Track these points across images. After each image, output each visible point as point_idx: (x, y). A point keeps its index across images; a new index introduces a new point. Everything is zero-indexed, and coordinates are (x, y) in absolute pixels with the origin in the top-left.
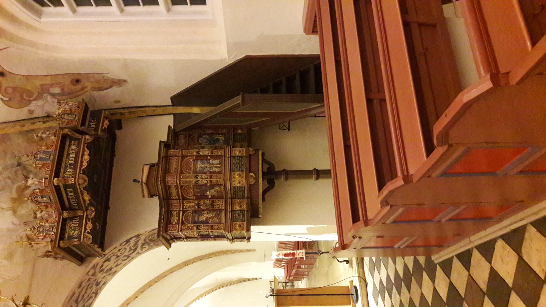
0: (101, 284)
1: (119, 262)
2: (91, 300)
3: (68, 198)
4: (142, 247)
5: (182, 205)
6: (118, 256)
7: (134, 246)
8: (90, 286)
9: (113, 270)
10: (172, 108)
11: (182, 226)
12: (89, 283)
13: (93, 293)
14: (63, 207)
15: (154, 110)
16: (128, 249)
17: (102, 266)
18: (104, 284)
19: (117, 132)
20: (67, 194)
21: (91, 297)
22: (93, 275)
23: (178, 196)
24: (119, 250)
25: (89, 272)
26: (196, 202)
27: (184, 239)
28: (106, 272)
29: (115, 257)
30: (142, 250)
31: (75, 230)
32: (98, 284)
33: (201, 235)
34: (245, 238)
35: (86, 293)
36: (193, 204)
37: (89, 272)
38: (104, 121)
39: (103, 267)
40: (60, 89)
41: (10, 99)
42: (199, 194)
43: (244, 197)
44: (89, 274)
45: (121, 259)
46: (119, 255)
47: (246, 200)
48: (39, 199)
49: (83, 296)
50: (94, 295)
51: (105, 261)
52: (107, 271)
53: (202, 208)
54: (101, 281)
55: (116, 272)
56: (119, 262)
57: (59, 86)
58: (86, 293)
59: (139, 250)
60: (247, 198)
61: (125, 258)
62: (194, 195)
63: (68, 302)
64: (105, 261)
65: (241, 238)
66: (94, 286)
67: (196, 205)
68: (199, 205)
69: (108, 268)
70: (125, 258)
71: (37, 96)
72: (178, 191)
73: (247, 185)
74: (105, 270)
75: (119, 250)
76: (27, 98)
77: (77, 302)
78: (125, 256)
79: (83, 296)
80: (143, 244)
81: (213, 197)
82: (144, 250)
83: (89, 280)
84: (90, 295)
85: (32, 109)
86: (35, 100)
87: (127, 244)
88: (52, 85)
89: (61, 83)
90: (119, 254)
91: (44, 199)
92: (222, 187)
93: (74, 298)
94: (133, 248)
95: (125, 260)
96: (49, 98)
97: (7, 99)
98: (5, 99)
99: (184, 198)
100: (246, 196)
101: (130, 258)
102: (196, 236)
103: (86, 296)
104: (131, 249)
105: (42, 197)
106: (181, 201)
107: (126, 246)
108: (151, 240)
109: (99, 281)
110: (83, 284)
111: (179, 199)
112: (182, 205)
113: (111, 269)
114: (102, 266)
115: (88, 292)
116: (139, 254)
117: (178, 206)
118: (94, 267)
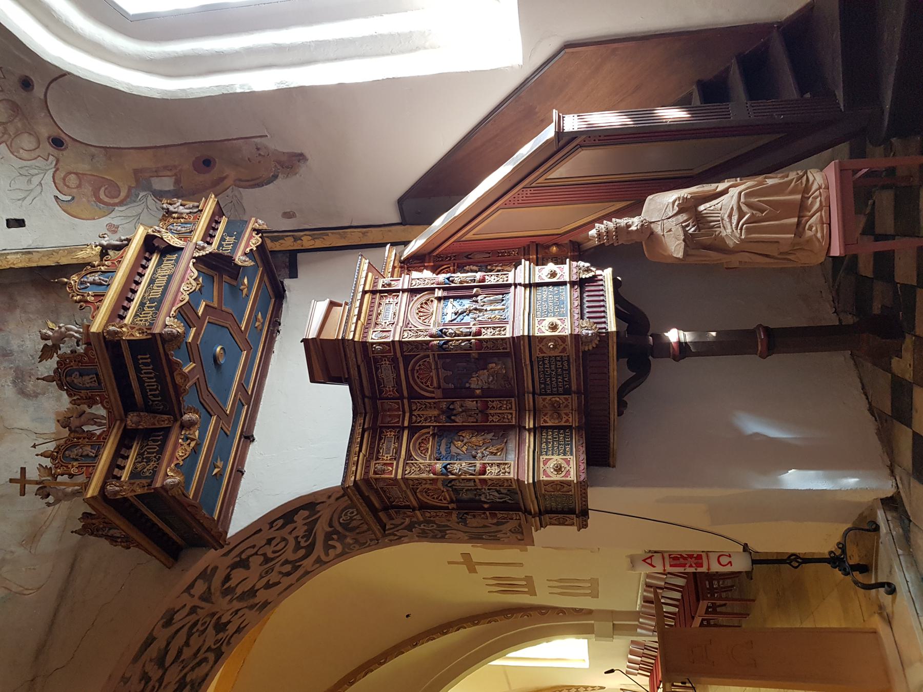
0: (231, 628)
1: (273, 577)
2: (205, 668)
3: (141, 382)
4: (327, 547)
5: (407, 415)
6: (267, 560)
7: (307, 536)
8: (199, 627)
9: (262, 596)
10: (402, 227)
11: (405, 464)
12: (193, 618)
13: (209, 649)
14: (129, 405)
15: (363, 233)
16: (292, 543)
17: (228, 578)
18: (239, 630)
19: (287, 282)
20: (138, 370)
21: (205, 660)
22: (206, 597)
23: (400, 390)
24: (269, 542)
25: (192, 586)
26: (444, 406)
27: (414, 509)
28: (241, 598)
29: (262, 558)
30: (327, 554)
31: (149, 460)
32: (220, 627)
33: (458, 501)
34: (572, 511)
35: (187, 644)
36: (436, 412)
37: (192, 586)
38: (251, 237)
39: (232, 583)
40: (173, 179)
41: (73, 198)
42: (451, 386)
43: (567, 392)
44: (192, 592)
45: (277, 568)
46: (270, 555)
47: (573, 400)
48: (77, 380)
49: (180, 652)
50: (211, 657)
51: (234, 566)
52: (241, 598)
53: (459, 421)
54: (229, 622)
55: (266, 604)
56: (273, 577)
57: (169, 173)
58: (187, 644)
59: (319, 550)
60: (578, 392)
61: (288, 568)
62: (439, 387)
63: (136, 659)
64: (234, 566)
65: (562, 512)
66: (211, 631)
67: (443, 412)
68: (449, 413)
69: (246, 586)
70: (288, 568)
71: (127, 197)
72: (399, 375)
73: (577, 351)
74: (239, 591)
75: (269, 542)
76: (106, 200)
77: (160, 661)
78: (287, 562)
79: (180, 652)
80: (328, 536)
81: (488, 393)
82: (332, 552)
83: (194, 610)
84: (200, 656)
85: (116, 222)
86: (121, 203)
87: (289, 527)
88: (157, 173)
89: (175, 167)
90: (269, 551)
91: (87, 378)
92: (509, 363)
93: (153, 651)
94: (303, 544)
95: (288, 574)
96: (150, 200)
97: (69, 198)
98: (61, 197)
99: (414, 396)
100: (574, 388)
101: (300, 572)
102: (444, 503)
103: (187, 653)
104: (298, 547)
105: (81, 375)
106: (406, 401)
107: (284, 532)
108: (345, 526)
109: (224, 620)
110: (177, 617)
111: (402, 398)
112: (407, 415)
113: (253, 592)
114: (228, 578)
115: (195, 641)
116: (321, 564)
117: (399, 416)
118: (206, 575)
